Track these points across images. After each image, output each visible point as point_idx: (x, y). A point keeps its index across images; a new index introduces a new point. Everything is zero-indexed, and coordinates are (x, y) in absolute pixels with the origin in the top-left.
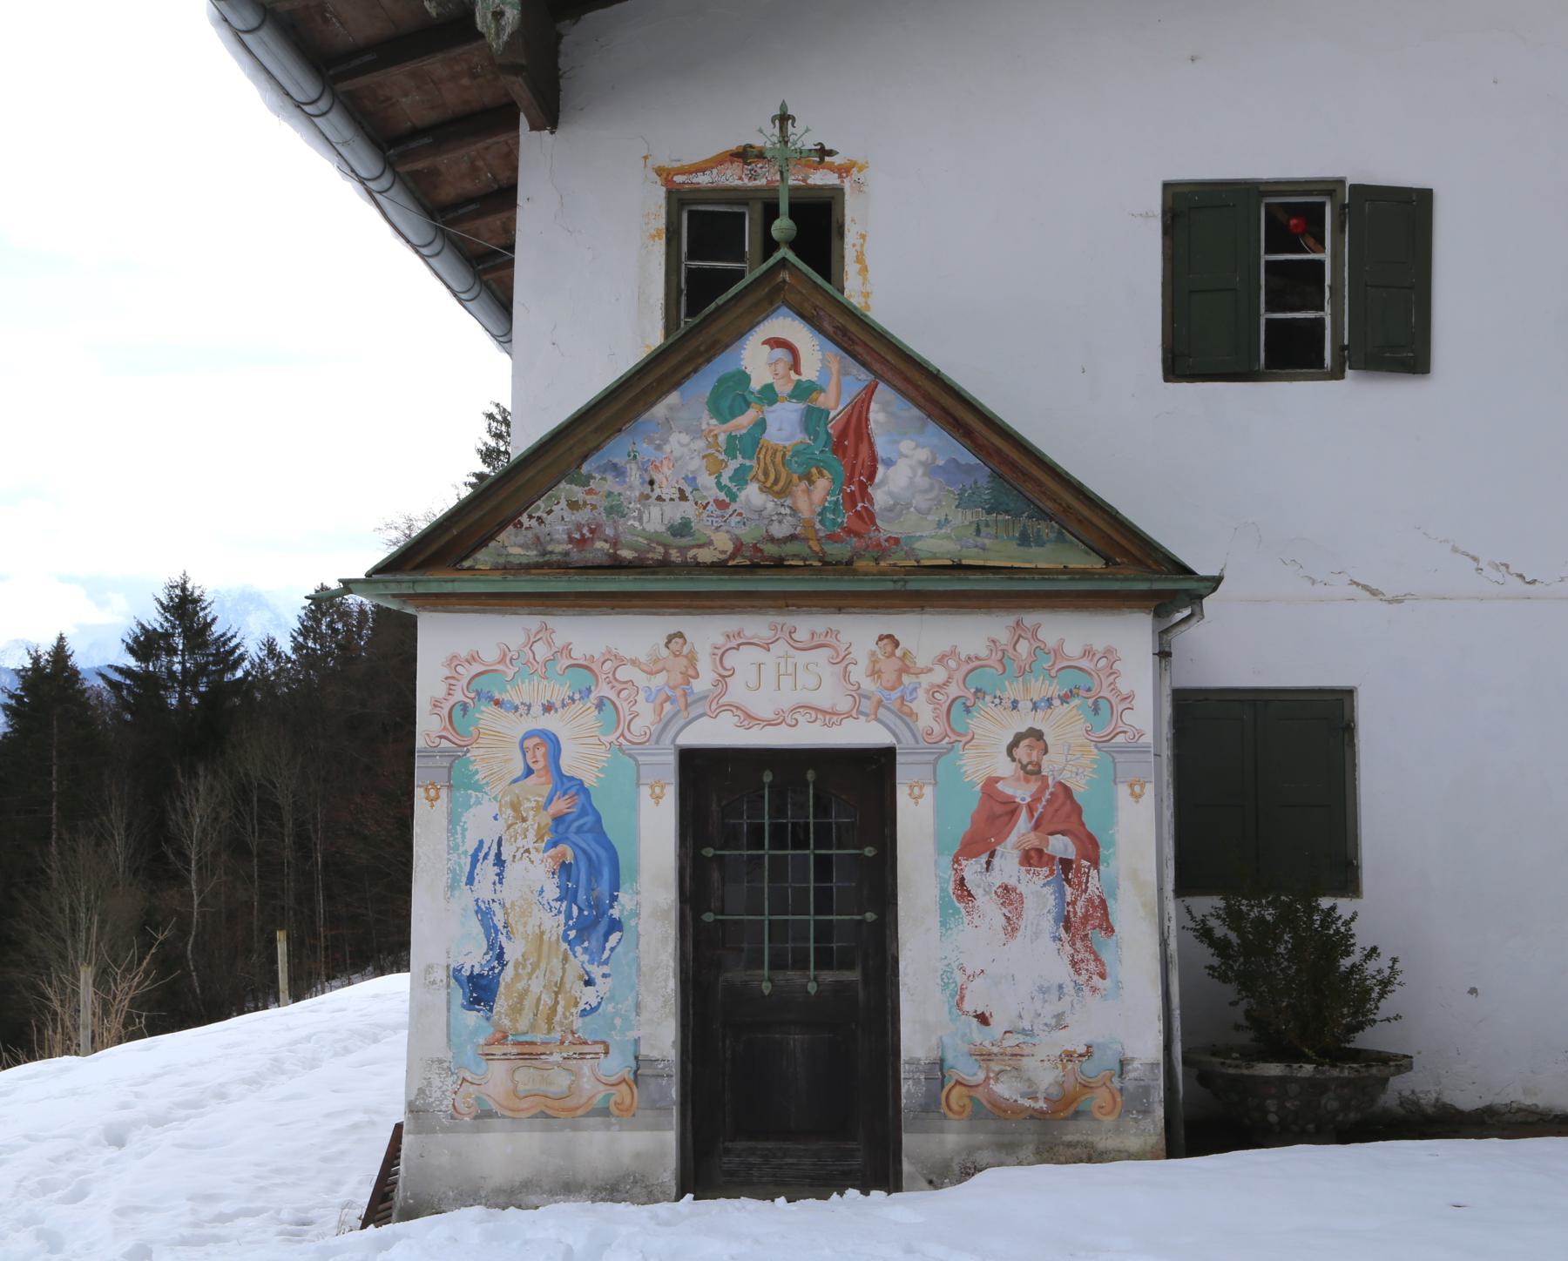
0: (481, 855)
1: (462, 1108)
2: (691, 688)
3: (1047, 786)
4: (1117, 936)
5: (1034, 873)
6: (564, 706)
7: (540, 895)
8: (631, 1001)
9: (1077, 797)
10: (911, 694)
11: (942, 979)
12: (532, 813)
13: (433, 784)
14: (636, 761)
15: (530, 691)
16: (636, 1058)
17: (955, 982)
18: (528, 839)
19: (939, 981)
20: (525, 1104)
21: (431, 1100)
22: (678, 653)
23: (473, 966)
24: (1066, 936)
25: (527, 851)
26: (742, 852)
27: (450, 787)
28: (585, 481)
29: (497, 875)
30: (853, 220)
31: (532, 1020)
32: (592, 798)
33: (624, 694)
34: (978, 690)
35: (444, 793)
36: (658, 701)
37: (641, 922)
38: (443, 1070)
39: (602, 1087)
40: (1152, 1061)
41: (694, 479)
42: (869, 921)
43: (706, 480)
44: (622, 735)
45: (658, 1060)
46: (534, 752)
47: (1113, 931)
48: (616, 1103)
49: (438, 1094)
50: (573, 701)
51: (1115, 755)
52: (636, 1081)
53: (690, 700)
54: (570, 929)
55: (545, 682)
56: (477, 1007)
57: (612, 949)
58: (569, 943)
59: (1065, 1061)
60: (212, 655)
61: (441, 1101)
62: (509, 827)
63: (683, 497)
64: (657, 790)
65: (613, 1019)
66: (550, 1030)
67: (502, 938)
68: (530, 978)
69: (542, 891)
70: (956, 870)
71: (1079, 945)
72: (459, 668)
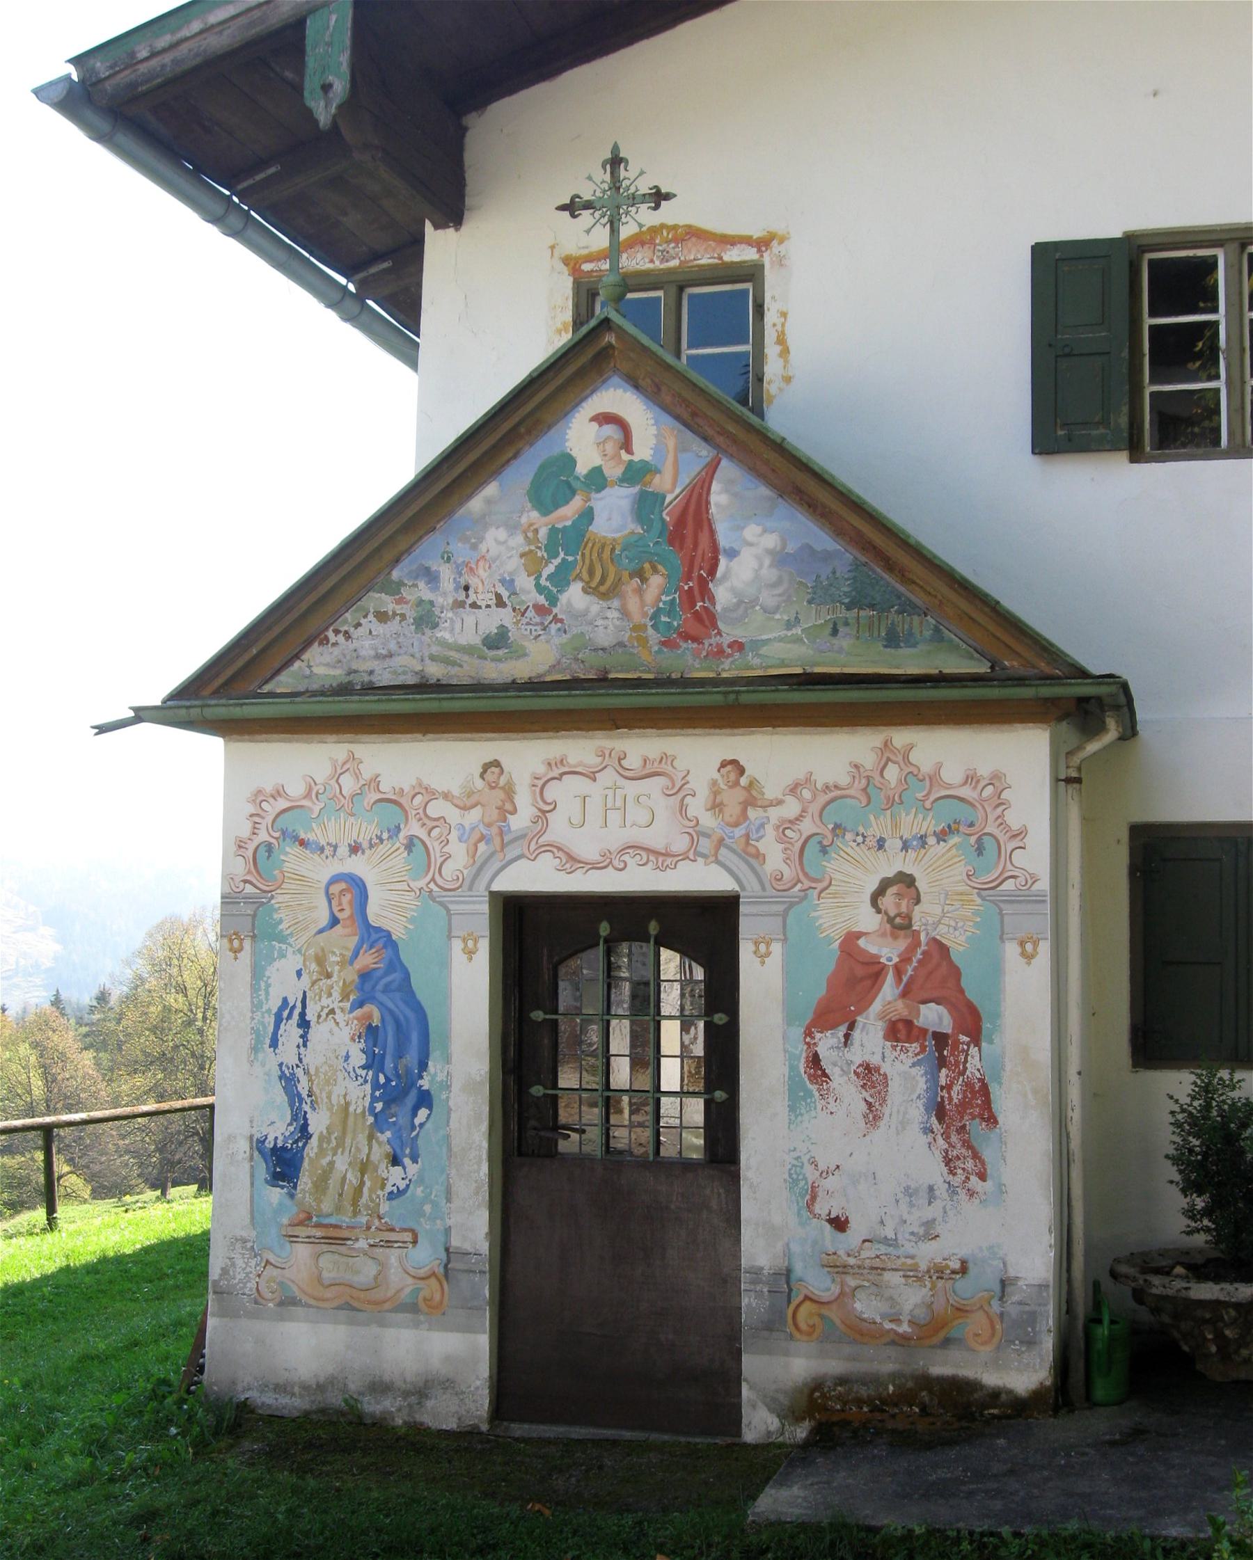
3: (919, 944)
4: (1000, 1128)
5: (901, 1050)
6: (371, 846)
7: (345, 1061)
9: (954, 956)
10: (758, 831)
11: (790, 1175)
14: (448, 910)
15: (334, 830)
16: (447, 1250)
17: (805, 1179)
19: (786, 1176)
20: (328, 1294)
23: (276, 1138)
24: (939, 1127)
27: (254, 937)
28: (394, 589)
29: (301, 1037)
30: (773, 298)
33: (435, 832)
34: (837, 826)
35: (247, 944)
36: (472, 841)
39: (410, 1280)
40: (1040, 1282)
41: (512, 581)
42: (719, 1101)
43: (525, 582)
44: (433, 879)
47: (996, 1122)
48: (425, 1299)
50: (382, 841)
51: (1002, 905)
55: (352, 819)
59: (934, 1278)
62: (314, 983)
63: (500, 603)
64: (470, 944)
66: (356, 1213)
67: (306, 1108)
68: (335, 1154)
69: (347, 1057)
70: (808, 1044)
71: (954, 1138)
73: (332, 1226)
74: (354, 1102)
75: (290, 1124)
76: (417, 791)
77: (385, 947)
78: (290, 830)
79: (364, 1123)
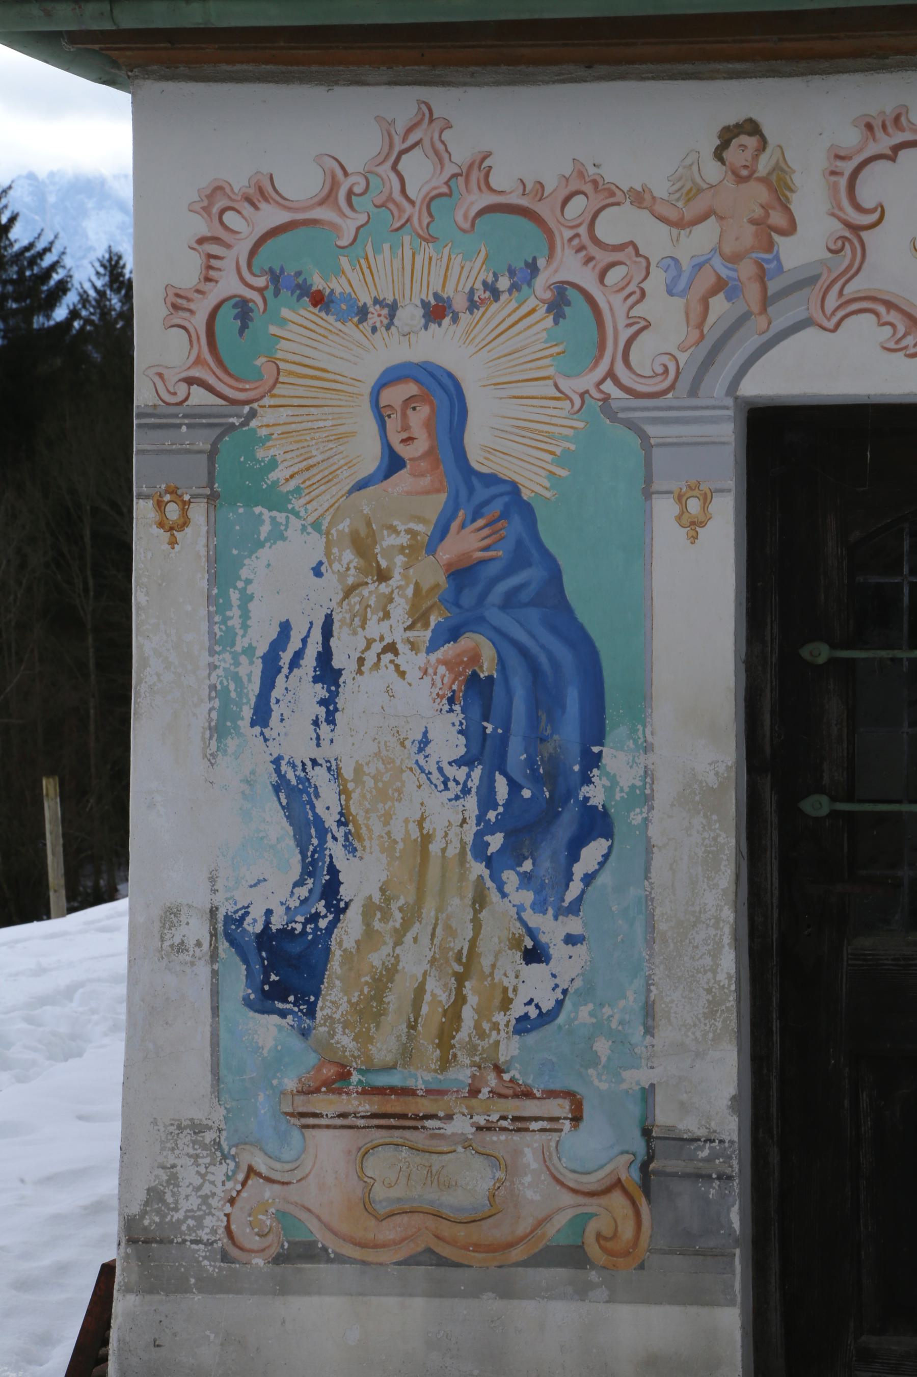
0: (286, 657)
1: (252, 1241)
2: (777, 258)
6: (473, 306)
7: (421, 750)
8: (632, 1000)
12: (400, 560)
13: (173, 491)
14: (644, 437)
16: (646, 1133)
18: (392, 621)
20: (389, 1232)
21: (177, 1216)
22: (745, 173)
23: (269, 913)
25: (391, 648)
26: (898, 654)
27: (213, 498)
29: (322, 702)
31: (404, 1039)
32: (541, 527)
33: (614, 276)
35: (198, 513)
37: (655, 815)
38: (204, 1147)
39: (567, 1198)
44: (610, 374)
45: (698, 1140)
46: (404, 415)
48: (599, 1236)
49: (194, 1202)
50: (496, 294)
52: (646, 1187)
53: (773, 287)
54: (491, 829)
55: (430, 249)
56: (280, 1005)
57: (588, 879)
58: (489, 862)
60: (11, 281)
61: (200, 1220)
62: (349, 592)
64: (694, 506)
65: (590, 1039)
66: (446, 1063)
67: (336, 849)
68: (398, 943)
69: (425, 742)
72: (229, 217)
73: (394, 1090)
74: (439, 834)
75: (299, 883)
76: (573, 187)
77: (505, 515)
78: (290, 270)
79: (462, 877)
